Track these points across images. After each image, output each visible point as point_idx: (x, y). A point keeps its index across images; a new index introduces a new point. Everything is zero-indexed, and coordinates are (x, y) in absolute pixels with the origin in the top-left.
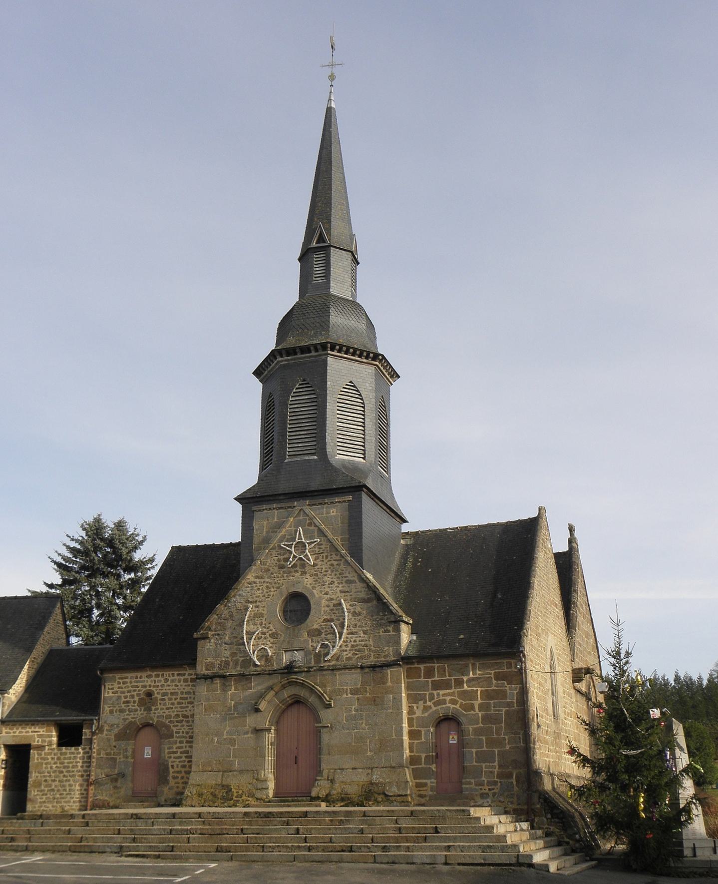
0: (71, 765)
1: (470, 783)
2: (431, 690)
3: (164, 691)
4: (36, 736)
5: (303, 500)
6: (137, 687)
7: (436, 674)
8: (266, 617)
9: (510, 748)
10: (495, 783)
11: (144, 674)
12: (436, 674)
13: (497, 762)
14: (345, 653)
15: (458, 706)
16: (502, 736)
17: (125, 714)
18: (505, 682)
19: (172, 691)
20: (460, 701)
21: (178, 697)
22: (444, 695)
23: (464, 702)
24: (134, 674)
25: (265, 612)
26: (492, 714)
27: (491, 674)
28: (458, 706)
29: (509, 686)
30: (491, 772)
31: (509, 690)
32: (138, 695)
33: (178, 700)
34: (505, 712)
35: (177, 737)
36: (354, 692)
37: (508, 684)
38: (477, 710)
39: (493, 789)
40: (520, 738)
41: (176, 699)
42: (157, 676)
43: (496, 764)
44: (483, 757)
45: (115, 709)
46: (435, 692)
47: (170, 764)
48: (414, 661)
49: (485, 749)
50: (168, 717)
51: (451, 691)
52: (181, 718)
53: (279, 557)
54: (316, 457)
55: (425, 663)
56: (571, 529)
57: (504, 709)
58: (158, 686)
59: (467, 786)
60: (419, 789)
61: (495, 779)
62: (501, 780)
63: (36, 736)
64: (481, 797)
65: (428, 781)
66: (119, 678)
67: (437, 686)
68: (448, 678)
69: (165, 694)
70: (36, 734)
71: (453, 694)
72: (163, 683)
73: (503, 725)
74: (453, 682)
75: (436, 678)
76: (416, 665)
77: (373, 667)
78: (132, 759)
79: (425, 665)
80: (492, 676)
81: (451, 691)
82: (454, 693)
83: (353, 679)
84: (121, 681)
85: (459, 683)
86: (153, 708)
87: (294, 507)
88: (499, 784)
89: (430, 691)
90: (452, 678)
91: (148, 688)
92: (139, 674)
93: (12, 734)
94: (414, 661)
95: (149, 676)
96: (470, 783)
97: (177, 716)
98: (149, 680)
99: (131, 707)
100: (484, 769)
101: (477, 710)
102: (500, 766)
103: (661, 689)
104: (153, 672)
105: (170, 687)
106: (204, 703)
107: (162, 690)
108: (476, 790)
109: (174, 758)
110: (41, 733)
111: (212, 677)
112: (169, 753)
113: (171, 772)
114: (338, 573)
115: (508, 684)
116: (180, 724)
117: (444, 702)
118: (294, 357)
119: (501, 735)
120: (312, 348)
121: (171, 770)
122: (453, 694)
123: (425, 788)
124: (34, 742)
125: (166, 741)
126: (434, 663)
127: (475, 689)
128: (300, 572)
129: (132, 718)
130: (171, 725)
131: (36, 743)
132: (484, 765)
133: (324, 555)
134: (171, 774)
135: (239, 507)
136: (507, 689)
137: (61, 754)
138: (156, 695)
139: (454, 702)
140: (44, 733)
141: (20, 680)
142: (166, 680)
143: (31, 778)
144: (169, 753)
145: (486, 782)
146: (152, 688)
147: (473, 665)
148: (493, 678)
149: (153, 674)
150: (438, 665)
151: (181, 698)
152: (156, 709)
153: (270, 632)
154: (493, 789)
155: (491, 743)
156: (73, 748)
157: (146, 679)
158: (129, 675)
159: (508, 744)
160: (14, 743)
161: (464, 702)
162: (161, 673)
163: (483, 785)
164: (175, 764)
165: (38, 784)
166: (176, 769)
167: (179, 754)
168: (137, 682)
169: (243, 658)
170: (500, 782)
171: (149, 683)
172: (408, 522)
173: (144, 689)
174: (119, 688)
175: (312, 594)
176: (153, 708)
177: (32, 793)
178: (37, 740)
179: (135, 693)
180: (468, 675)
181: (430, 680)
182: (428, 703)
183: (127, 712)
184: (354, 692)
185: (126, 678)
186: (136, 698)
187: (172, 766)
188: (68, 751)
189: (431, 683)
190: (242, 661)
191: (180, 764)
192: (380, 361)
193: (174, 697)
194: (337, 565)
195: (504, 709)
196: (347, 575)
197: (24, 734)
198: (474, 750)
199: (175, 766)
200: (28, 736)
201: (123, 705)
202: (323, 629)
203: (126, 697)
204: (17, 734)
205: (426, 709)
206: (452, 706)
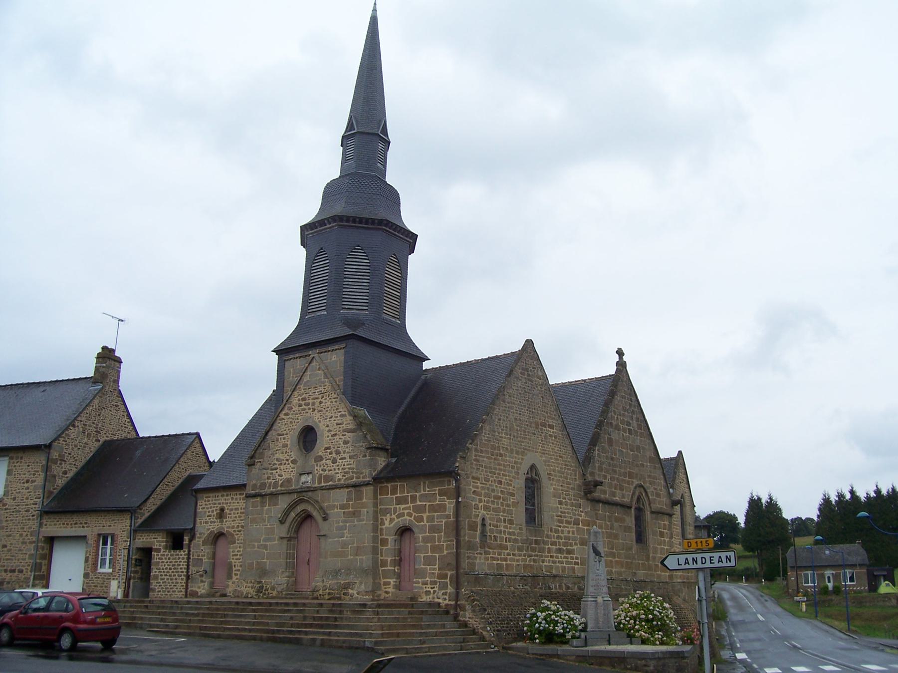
0: (176, 564)
1: (419, 583)
2: (396, 505)
3: (231, 507)
4: (156, 542)
5: (315, 349)
6: (215, 504)
7: (399, 492)
8: (289, 447)
9: (448, 553)
10: (435, 583)
11: (220, 494)
12: (399, 492)
13: (437, 565)
14: (337, 475)
15: (412, 519)
16: (442, 543)
17: (208, 525)
18: (446, 498)
19: (236, 507)
20: (414, 514)
21: (239, 512)
22: (404, 509)
23: (417, 515)
24: (214, 495)
25: (289, 443)
26: (436, 525)
27: (436, 490)
28: (412, 519)
29: (448, 500)
30: (433, 573)
31: (448, 504)
32: (216, 510)
33: (239, 514)
34: (444, 523)
35: (237, 543)
36: (342, 507)
37: (447, 499)
38: (425, 522)
39: (434, 588)
40: (454, 544)
41: (238, 513)
42: (227, 495)
43: (437, 566)
44: (429, 561)
45: (202, 521)
46: (398, 506)
47: (233, 564)
48: (383, 480)
49: (430, 554)
50: (233, 527)
51: (408, 505)
52: (240, 528)
53: (299, 397)
54: (326, 313)
55: (391, 482)
56: (620, 353)
57: (444, 521)
58: (228, 503)
59: (416, 585)
60: (385, 587)
61: (436, 580)
62: (440, 580)
63: (156, 542)
64: (425, 594)
65: (391, 581)
66: (206, 497)
67: (400, 501)
68: (406, 494)
69: (232, 510)
70: (156, 540)
71: (409, 508)
72: (230, 501)
73: (443, 534)
74: (410, 497)
75: (398, 495)
76: (385, 485)
77: (354, 486)
78: (804, 596)
79: (393, 484)
80: (437, 492)
81: (408, 505)
82: (410, 507)
83: (340, 497)
84: (207, 499)
85: (414, 499)
86: (224, 520)
87: (310, 355)
88: (438, 583)
89: (394, 506)
90: (409, 494)
91: (222, 505)
92: (217, 495)
93: (141, 540)
94: (383, 480)
95: (222, 496)
96: (419, 583)
97: (238, 526)
98: (223, 499)
99: (212, 520)
100: (428, 571)
101: (425, 522)
102: (439, 569)
103: (773, 504)
104: (225, 492)
105: (235, 504)
106: (250, 517)
107: (230, 506)
108: (422, 588)
109: (236, 559)
110: (159, 539)
111: (255, 496)
112: (233, 555)
113: (234, 570)
114: (335, 408)
115: (447, 499)
116: (239, 533)
117: (403, 515)
118: (315, 230)
119: (441, 542)
120: (326, 222)
121: (234, 569)
122: (409, 508)
123: (389, 586)
124: (154, 546)
125: (232, 546)
126: (397, 482)
127: (425, 503)
128: (312, 409)
129: (213, 528)
130: (235, 533)
131: (155, 547)
132: (428, 567)
133: (327, 394)
134: (234, 572)
135: (275, 357)
136: (447, 503)
137: (171, 555)
138: (226, 510)
139: (410, 515)
140: (161, 539)
141: (153, 499)
142: (232, 498)
143: (152, 572)
144: (233, 555)
145: (429, 581)
146: (224, 505)
147: (424, 483)
148: (396, 496)
149: (225, 494)
150: (400, 483)
151: (241, 512)
152: (226, 522)
153: (292, 459)
154: (434, 588)
155: (435, 549)
156: (178, 551)
157: (221, 498)
158: (211, 495)
159: (446, 550)
160: (142, 547)
161: (417, 515)
162: (229, 493)
163: (427, 584)
164: (236, 564)
165: (156, 577)
166: (237, 568)
167: (238, 557)
168: (216, 500)
169: (274, 481)
170: (439, 582)
171: (223, 501)
172: (429, 360)
173: (219, 506)
174: (205, 505)
175: (318, 427)
176: (224, 520)
177: (154, 584)
178: (156, 544)
179: (214, 509)
180: (420, 492)
181: (394, 496)
182: (394, 516)
183: (210, 524)
184: (342, 507)
185: (209, 497)
186: (215, 513)
187: (235, 565)
188: (175, 553)
189: (395, 499)
190: (274, 483)
191: (239, 564)
192: (386, 225)
193: (236, 512)
194: (335, 402)
195: (444, 521)
196: (341, 410)
197: (148, 540)
198: (422, 555)
199: (236, 566)
200: (150, 541)
201: (207, 518)
202: (324, 455)
203: (209, 512)
204: (144, 540)
205: (391, 520)
206: (408, 518)
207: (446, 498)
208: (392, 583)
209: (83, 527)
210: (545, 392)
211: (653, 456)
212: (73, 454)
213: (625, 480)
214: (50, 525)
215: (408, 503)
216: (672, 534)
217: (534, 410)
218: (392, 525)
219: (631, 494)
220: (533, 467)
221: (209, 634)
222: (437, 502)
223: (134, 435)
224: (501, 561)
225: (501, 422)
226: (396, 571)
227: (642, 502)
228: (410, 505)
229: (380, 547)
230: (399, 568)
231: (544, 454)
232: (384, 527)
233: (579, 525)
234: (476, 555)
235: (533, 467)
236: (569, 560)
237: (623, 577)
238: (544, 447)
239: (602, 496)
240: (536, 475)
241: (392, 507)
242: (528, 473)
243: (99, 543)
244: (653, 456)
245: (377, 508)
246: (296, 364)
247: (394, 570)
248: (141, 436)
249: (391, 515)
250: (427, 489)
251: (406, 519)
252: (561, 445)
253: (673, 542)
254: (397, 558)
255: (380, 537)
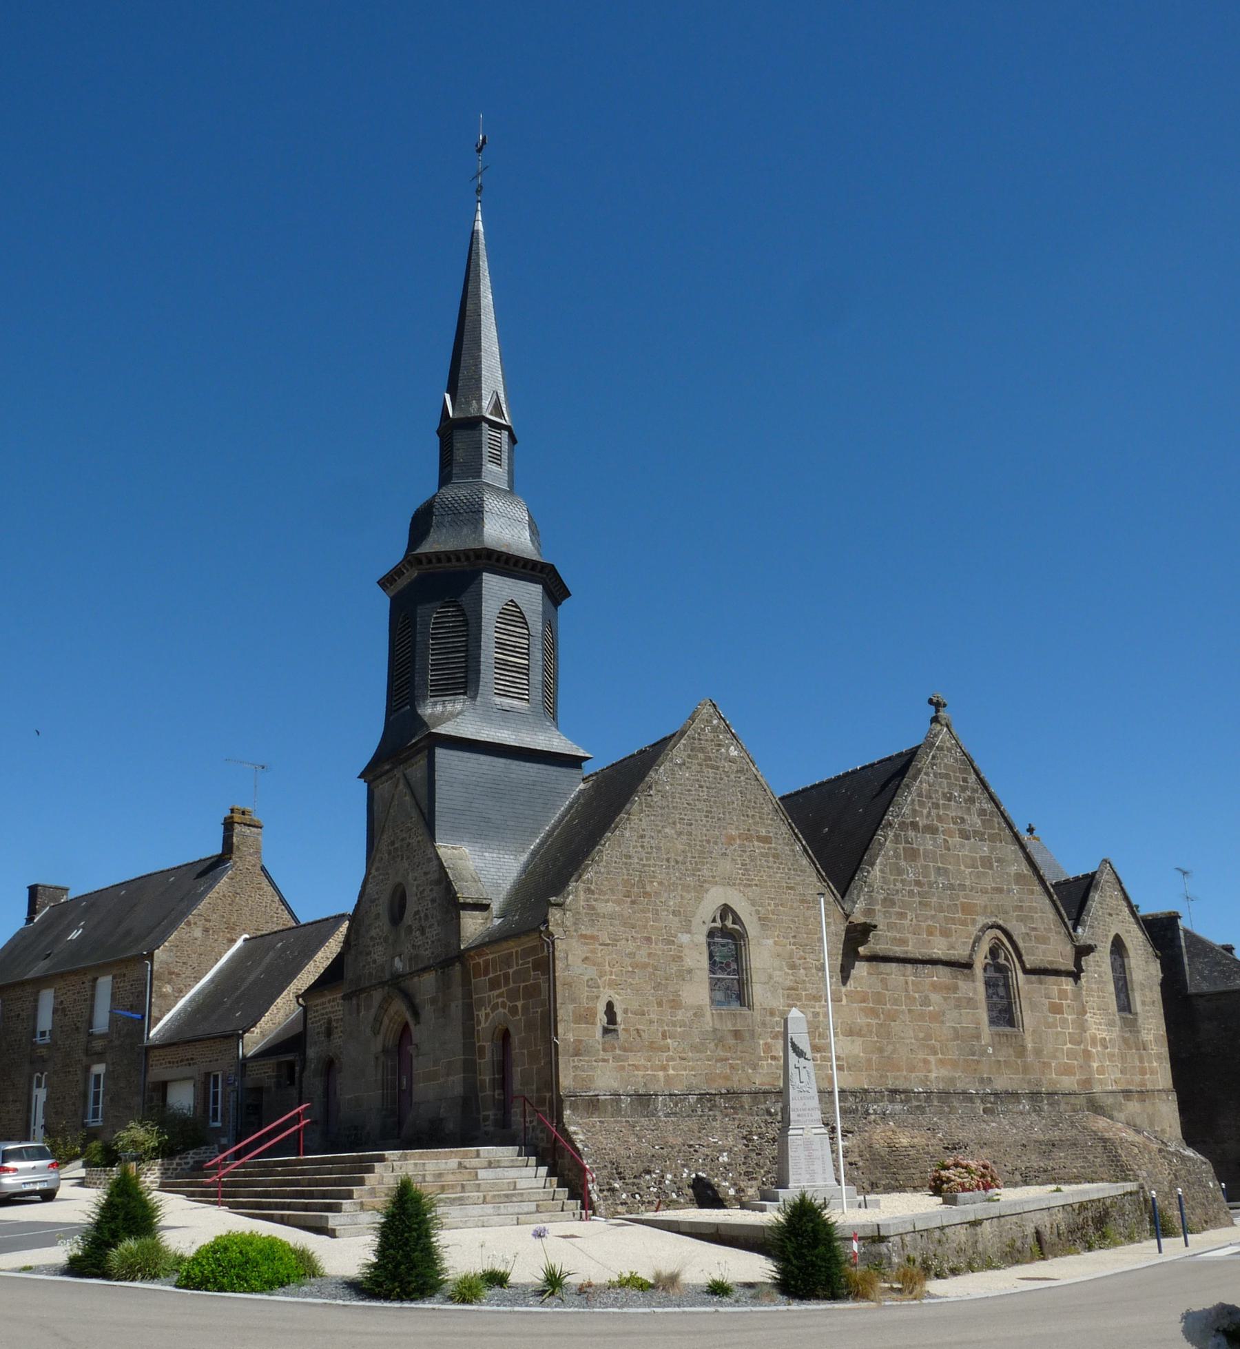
27: (528, 962)
51: (501, 991)
81: (501, 991)
207: (539, 972)
208: (492, 1117)
209: (190, 1064)
210: (747, 783)
211: (1026, 872)
212: (190, 963)
213: (953, 919)
214: (156, 1065)
215: (501, 988)
216: (1084, 1007)
217: (721, 815)
218: (487, 1024)
219: (971, 941)
220: (726, 910)
221: (272, 1215)
222: (532, 982)
223: (286, 921)
224: (652, 1071)
225: (646, 840)
226: (496, 1097)
227: (1003, 954)
228: (503, 989)
229: (478, 1061)
230: (501, 1091)
231: (750, 886)
232: (480, 1028)
233: (841, 1001)
234: (595, 1064)
235: (726, 910)
236: (819, 1062)
237: (960, 1086)
238: (749, 875)
239: (897, 949)
240: (734, 923)
241: (486, 995)
242: (714, 921)
243: (209, 1084)
244: (1026, 872)
245: (472, 998)
246: (384, 788)
247: (494, 1096)
248: (303, 922)
249: (485, 1009)
250: (521, 962)
251: (500, 1012)
252: (790, 869)
253: (1087, 1020)
254: (496, 1076)
255: (477, 1044)
